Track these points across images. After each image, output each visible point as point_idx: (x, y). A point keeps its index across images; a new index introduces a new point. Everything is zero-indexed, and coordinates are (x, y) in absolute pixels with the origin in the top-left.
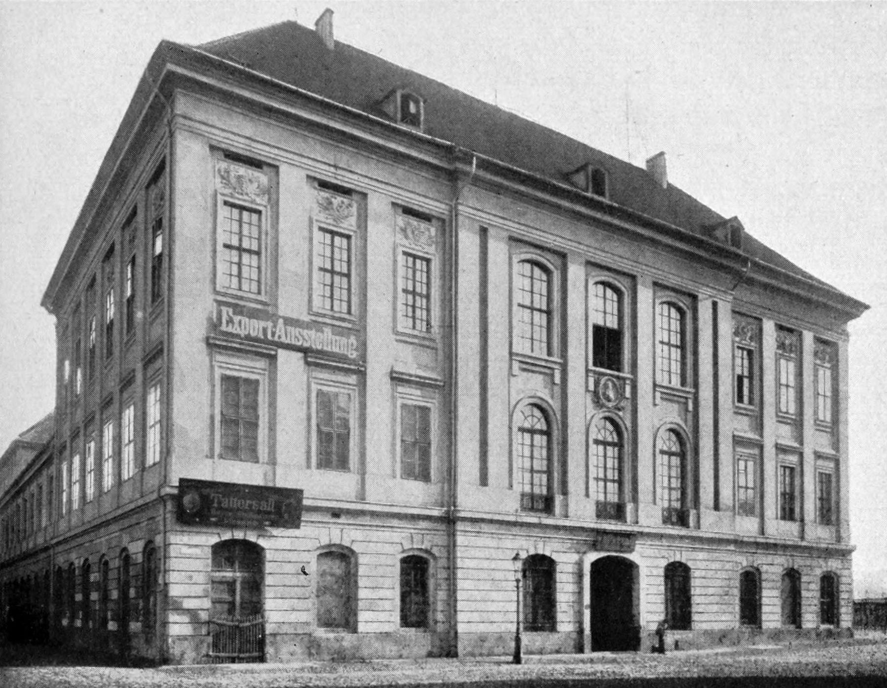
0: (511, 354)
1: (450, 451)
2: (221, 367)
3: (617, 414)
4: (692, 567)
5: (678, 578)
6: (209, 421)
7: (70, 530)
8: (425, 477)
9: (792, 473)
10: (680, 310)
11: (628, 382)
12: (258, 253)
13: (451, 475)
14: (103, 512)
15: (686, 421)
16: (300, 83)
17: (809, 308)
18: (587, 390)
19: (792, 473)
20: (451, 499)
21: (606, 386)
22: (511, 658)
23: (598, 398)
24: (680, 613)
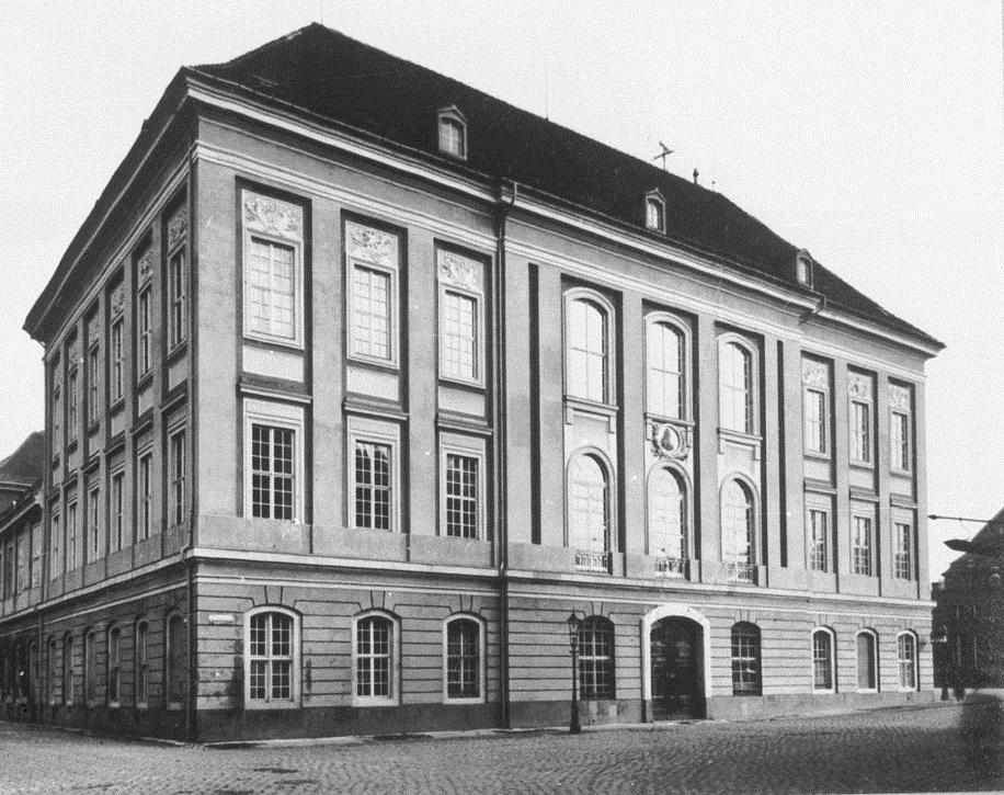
0: (565, 399)
1: (628, 590)
2: (250, 417)
3: (679, 465)
4: (761, 627)
5: (747, 637)
6: (919, 498)
7: (15, 613)
8: (471, 533)
9: (874, 526)
10: (746, 353)
11: (689, 429)
12: (348, 362)
13: (498, 528)
14: (19, 608)
15: (752, 470)
16: (333, 89)
17: (916, 343)
18: (645, 438)
19: (874, 526)
20: (500, 555)
21: (667, 434)
22: (567, 728)
23: (658, 447)
24: (749, 679)
